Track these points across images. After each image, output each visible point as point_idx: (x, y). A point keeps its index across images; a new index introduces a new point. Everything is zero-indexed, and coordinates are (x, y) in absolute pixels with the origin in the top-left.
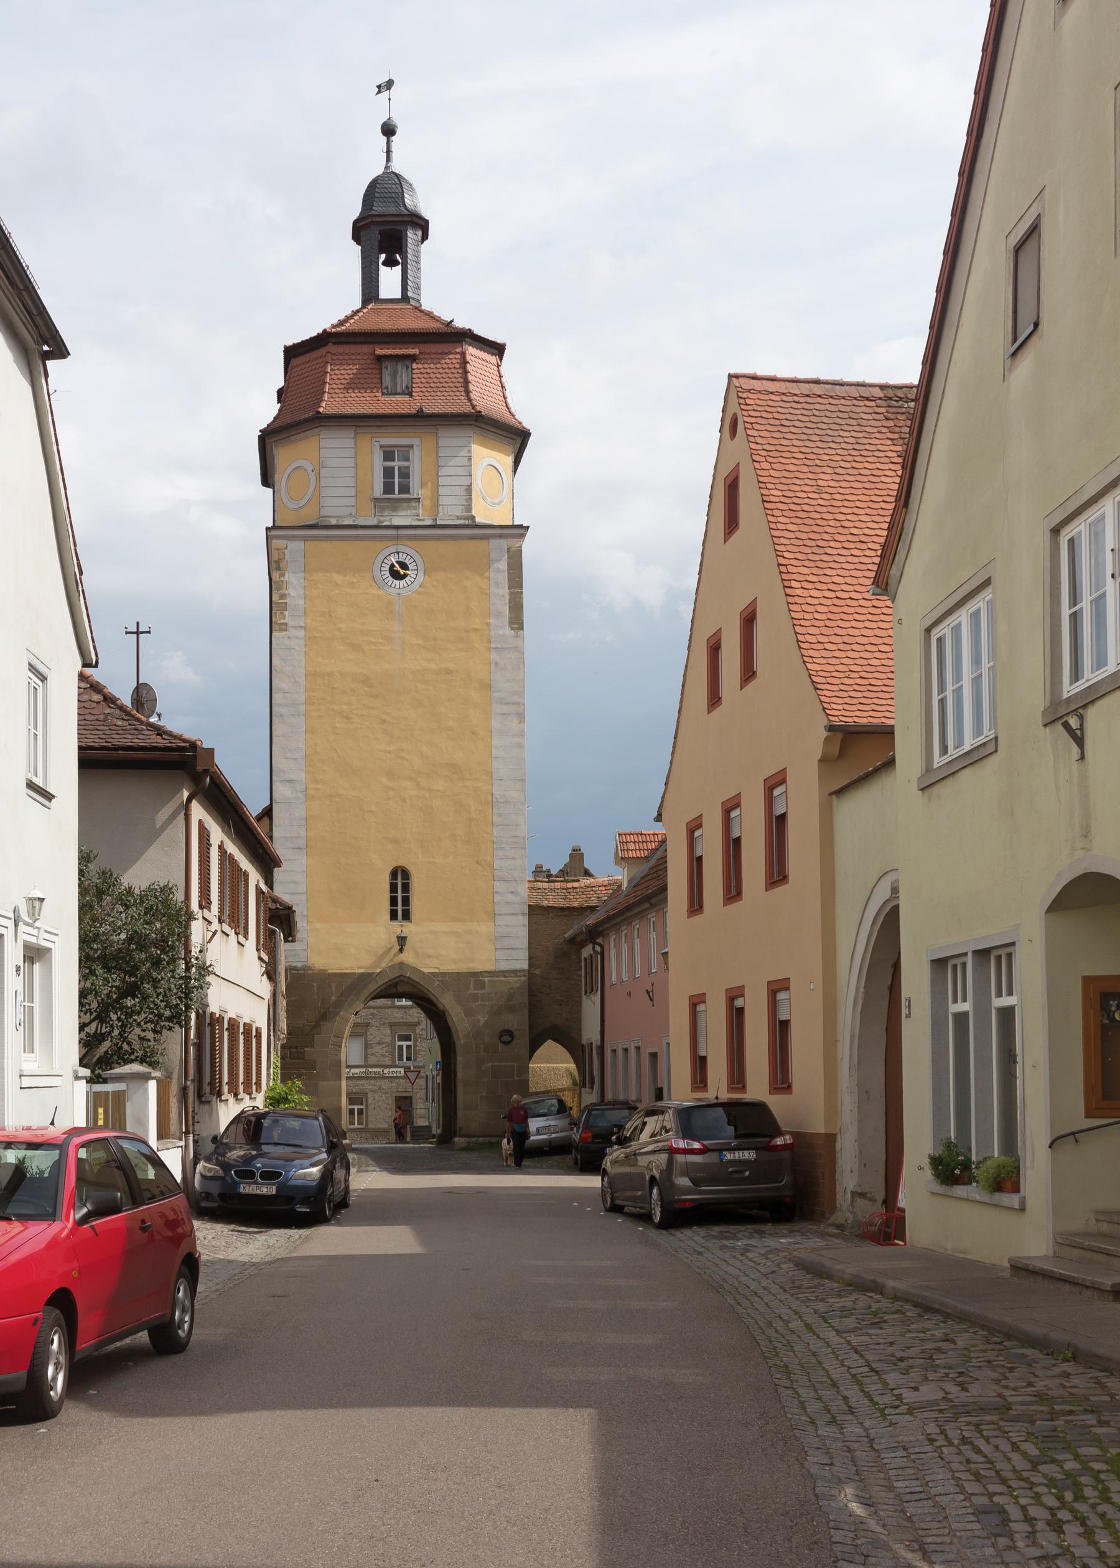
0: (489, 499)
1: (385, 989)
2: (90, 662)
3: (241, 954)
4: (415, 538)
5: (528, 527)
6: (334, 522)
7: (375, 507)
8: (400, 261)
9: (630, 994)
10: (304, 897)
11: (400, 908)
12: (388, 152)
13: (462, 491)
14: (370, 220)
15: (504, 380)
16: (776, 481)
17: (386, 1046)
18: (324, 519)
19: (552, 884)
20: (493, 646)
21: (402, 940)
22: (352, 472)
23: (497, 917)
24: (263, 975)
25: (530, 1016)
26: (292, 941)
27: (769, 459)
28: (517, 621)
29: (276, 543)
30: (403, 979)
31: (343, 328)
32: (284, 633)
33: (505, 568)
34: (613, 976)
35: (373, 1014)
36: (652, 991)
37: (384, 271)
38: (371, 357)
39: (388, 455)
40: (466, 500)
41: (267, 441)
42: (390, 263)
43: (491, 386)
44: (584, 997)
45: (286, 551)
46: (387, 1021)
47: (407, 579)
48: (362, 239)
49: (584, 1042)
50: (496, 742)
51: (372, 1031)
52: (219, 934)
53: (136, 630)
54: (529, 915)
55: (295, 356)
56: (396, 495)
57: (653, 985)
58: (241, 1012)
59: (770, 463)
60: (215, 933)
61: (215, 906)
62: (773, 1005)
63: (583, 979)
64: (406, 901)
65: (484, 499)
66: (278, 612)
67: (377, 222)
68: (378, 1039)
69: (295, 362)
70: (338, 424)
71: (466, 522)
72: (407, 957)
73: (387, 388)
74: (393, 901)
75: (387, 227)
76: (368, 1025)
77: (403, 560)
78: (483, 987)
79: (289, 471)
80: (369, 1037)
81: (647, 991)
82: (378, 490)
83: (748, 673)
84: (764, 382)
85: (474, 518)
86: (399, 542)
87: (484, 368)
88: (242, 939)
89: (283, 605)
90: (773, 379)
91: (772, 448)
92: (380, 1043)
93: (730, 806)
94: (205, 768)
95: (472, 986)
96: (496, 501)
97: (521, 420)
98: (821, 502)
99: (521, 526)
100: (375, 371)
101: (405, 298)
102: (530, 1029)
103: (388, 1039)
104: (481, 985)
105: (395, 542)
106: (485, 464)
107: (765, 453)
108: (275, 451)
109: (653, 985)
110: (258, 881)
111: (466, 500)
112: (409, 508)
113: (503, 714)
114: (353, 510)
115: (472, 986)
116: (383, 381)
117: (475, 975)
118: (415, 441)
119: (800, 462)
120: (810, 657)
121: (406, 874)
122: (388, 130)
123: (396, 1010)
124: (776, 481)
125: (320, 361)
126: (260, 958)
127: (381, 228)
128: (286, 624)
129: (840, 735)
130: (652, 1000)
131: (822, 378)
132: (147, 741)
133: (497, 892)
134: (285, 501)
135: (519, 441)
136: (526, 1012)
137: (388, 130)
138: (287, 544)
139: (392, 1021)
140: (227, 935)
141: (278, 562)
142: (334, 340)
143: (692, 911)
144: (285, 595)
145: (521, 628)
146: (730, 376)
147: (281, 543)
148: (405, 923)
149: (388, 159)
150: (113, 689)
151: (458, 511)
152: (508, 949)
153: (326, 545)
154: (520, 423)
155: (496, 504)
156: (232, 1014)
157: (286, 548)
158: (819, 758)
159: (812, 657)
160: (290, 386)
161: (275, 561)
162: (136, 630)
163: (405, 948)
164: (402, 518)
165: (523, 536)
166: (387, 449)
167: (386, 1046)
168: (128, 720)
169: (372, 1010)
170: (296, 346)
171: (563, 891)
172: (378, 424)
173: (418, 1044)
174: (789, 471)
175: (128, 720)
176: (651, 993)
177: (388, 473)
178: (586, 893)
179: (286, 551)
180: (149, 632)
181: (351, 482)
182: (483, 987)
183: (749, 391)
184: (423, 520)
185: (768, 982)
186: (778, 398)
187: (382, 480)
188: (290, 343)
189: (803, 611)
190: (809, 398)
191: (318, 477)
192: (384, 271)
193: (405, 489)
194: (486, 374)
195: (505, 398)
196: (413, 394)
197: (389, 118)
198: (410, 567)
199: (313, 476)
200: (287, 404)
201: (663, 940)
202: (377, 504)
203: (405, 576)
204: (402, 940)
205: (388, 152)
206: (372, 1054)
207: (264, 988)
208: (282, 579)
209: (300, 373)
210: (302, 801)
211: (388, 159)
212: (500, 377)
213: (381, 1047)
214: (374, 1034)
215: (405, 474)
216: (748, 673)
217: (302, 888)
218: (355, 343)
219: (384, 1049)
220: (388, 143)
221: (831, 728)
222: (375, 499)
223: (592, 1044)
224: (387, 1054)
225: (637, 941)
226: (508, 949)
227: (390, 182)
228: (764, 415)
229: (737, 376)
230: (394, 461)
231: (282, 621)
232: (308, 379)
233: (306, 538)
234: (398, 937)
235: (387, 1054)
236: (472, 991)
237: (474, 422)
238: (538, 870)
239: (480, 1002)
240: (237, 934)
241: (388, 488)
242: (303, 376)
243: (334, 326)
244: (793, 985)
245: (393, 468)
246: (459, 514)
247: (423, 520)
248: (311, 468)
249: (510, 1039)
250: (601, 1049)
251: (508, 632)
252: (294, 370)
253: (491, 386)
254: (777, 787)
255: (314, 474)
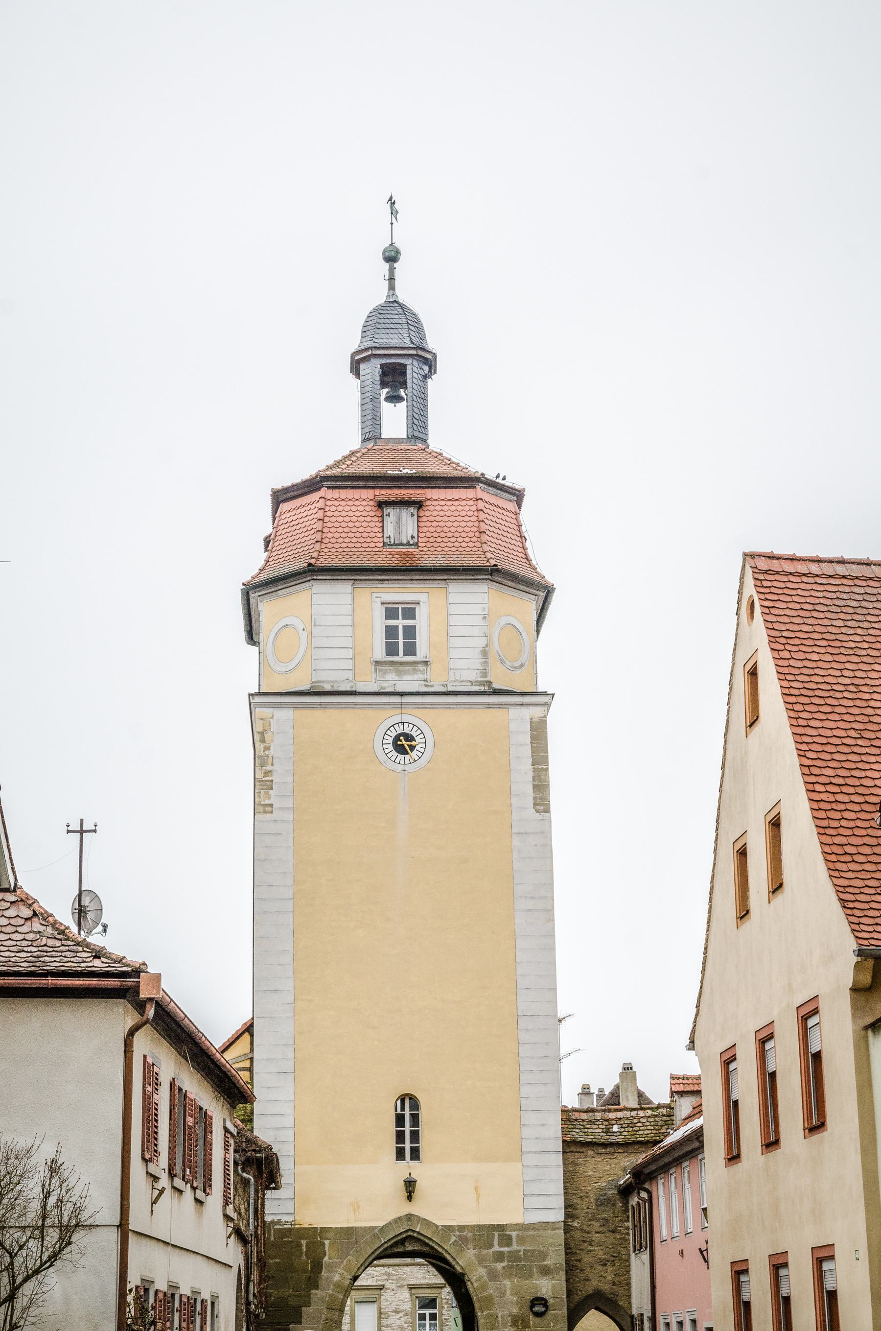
0: (508, 663)
1: (391, 1246)
2: (7, 886)
3: (200, 1214)
4: (423, 706)
5: (553, 695)
6: (328, 688)
7: (376, 671)
8: (405, 397)
9: (682, 1253)
10: (291, 1132)
11: (408, 1145)
12: (392, 279)
13: (477, 653)
14: (370, 353)
15: (523, 528)
16: (797, 671)
17: (405, 1316)
18: (319, 684)
19: (591, 1114)
20: (515, 830)
21: (410, 1186)
22: (349, 632)
23: (525, 1156)
24: (229, 1237)
25: (567, 1280)
26: (274, 1188)
27: (788, 647)
28: (542, 803)
29: (258, 711)
30: (412, 1234)
31: (339, 470)
32: (269, 815)
33: (528, 740)
34: (662, 1230)
35: (388, 1274)
36: (707, 1250)
37: (387, 408)
38: (371, 503)
39: (391, 613)
40: (481, 663)
41: (251, 595)
42: (394, 398)
43: (509, 535)
44: (633, 1255)
45: (272, 721)
46: (406, 1283)
47: (407, 757)
48: (361, 373)
49: (635, 1312)
50: (520, 943)
51: (387, 1295)
52: (168, 1192)
53: (79, 829)
54: (564, 1152)
55: (284, 501)
56: (401, 658)
57: (707, 1242)
58: (197, 1286)
59: (790, 651)
60: (162, 1192)
61: (163, 1160)
62: (820, 1276)
63: (631, 1232)
64: (415, 1136)
65: (502, 662)
66: (262, 791)
67: (376, 355)
68: (394, 1306)
69: (284, 507)
70: (333, 577)
71: (482, 688)
72: (418, 1209)
73: (389, 537)
74: (400, 1137)
75: (389, 361)
76: (381, 1288)
77: (409, 732)
78: (509, 1244)
79: (275, 630)
80: (384, 1304)
81: (700, 1249)
82: (379, 652)
83: (777, 887)
84: (782, 562)
85: (490, 683)
86: (404, 711)
87: (500, 516)
88: (200, 1194)
89: (268, 783)
90: (793, 559)
91: (792, 635)
92: (397, 1312)
93: (764, 1039)
94: (149, 996)
95: (496, 1242)
96: (517, 664)
97: (544, 573)
98: (846, 694)
99: (545, 694)
100: (376, 519)
101: (412, 438)
102: (568, 1295)
103: (407, 1306)
104: (506, 1240)
105: (399, 711)
106: (503, 621)
107: (783, 641)
108: (261, 606)
109: (707, 1242)
110: (225, 1120)
111: (481, 663)
112: (415, 671)
113: (529, 910)
114: (350, 675)
115: (496, 1242)
116: (385, 530)
117: (501, 1228)
118: (422, 597)
119: (823, 650)
120: (836, 870)
121: (415, 1104)
122: (392, 257)
123: (417, 1268)
124: (797, 671)
125: (313, 506)
126: (227, 1217)
127: (384, 361)
128: (271, 805)
129: (870, 962)
130: (706, 1261)
131: (846, 557)
132: (82, 965)
133: (524, 1125)
134: (272, 663)
135: (800, 1008)
136: (563, 1274)
137: (392, 257)
138: (273, 713)
139: (411, 1283)
140: (180, 1192)
141: (262, 734)
142: (328, 484)
143: (730, 1160)
144: (271, 772)
145: (547, 811)
146: (745, 555)
147: (267, 712)
148: (414, 1163)
149: (392, 287)
150: (46, 904)
151: (474, 676)
152: (539, 1195)
153: (318, 713)
154: (543, 577)
155: (515, 668)
156: (185, 1290)
157: (272, 717)
158: (850, 986)
159: (838, 870)
160: (278, 534)
161: (258, 733)
162: (79, 829)
163: (414, 1195)
164: (410, 682)
165: (547, 705)
166: (390, 606)
167: (405, 1316)
168: (61, 940)
169: (386, 1268)
170: (286, 490)
171: (605, 1123)
172: (380, 578)
173: (444, 1312)
174: (810, 660)
175: (61, 940)
176: (705, 1253)
177: (391, 632)
178: (632, 1125)
179: (272, 721)
180: (95, 831)
181: (349, 643)
182: (509, 1244)
183: (766, 572)
184: (432, 686)
185: (812, 1248)
186: (798, 580)
187: (384, 640)
188: (279, 486)
189: (828, 818)
190: (833, 579)
191: (309, 635)
192: (387, 408)
193: (410, 649)
194: (503, 523)
195: (525, 549)
196: (420, 544)
197: (391, 245)
198: (414, 734)
199: (304, 636)
200: (274, 554)
201: (699, 1195)
202: (378, 667)
203: (412, 748)
204: (410, 1186)
205: (392, 279)
206: (387, 1326)
207: (233, 1254)
208: (267, 752)
209: (290, 520)
210: (289, 1015)
211: (392, 287)
212: (519, 526)
213: (398, 1316)
214: (389, 1299)
215: (410, 632)
216: (777, 887)
217: (289, 1122)
218: (353, 487)
219: (403, 1319)
220: (392, 270)
221: (860, 953)
222: (376, 662)
223: (642, 1315)
224: (406, 1326)
225: (687, 1186)
226: (539, 1195)
227: (393, 312)
228: (782, 598)
229: (752, 556)
230: (398, 619)
231: (267, 802)
232: (299, 526)
233: (295, 706)
234: (405, 1181)
235: (406, 1326)
236: (496, 1248)
237: (489, 577)
238: (586, 1090)
239: (505, 1264)
240: (194, 1189)
241: (391, 650)
242: (293, 523)
243: (329, 468)
244: (838, 1252)
245: (397, 627)
246: (473, 678)
247: (432, 686)
248: (301, 627)
249: (544, 1309)
250: (653, 1319)
251: (531, 812)
252: (283, 517)
253: (509, 535)
254: (810, 1017)
255: (305, 632)
